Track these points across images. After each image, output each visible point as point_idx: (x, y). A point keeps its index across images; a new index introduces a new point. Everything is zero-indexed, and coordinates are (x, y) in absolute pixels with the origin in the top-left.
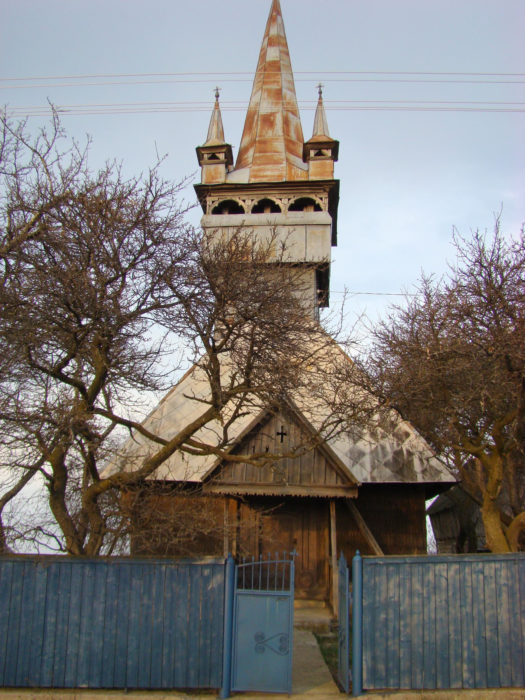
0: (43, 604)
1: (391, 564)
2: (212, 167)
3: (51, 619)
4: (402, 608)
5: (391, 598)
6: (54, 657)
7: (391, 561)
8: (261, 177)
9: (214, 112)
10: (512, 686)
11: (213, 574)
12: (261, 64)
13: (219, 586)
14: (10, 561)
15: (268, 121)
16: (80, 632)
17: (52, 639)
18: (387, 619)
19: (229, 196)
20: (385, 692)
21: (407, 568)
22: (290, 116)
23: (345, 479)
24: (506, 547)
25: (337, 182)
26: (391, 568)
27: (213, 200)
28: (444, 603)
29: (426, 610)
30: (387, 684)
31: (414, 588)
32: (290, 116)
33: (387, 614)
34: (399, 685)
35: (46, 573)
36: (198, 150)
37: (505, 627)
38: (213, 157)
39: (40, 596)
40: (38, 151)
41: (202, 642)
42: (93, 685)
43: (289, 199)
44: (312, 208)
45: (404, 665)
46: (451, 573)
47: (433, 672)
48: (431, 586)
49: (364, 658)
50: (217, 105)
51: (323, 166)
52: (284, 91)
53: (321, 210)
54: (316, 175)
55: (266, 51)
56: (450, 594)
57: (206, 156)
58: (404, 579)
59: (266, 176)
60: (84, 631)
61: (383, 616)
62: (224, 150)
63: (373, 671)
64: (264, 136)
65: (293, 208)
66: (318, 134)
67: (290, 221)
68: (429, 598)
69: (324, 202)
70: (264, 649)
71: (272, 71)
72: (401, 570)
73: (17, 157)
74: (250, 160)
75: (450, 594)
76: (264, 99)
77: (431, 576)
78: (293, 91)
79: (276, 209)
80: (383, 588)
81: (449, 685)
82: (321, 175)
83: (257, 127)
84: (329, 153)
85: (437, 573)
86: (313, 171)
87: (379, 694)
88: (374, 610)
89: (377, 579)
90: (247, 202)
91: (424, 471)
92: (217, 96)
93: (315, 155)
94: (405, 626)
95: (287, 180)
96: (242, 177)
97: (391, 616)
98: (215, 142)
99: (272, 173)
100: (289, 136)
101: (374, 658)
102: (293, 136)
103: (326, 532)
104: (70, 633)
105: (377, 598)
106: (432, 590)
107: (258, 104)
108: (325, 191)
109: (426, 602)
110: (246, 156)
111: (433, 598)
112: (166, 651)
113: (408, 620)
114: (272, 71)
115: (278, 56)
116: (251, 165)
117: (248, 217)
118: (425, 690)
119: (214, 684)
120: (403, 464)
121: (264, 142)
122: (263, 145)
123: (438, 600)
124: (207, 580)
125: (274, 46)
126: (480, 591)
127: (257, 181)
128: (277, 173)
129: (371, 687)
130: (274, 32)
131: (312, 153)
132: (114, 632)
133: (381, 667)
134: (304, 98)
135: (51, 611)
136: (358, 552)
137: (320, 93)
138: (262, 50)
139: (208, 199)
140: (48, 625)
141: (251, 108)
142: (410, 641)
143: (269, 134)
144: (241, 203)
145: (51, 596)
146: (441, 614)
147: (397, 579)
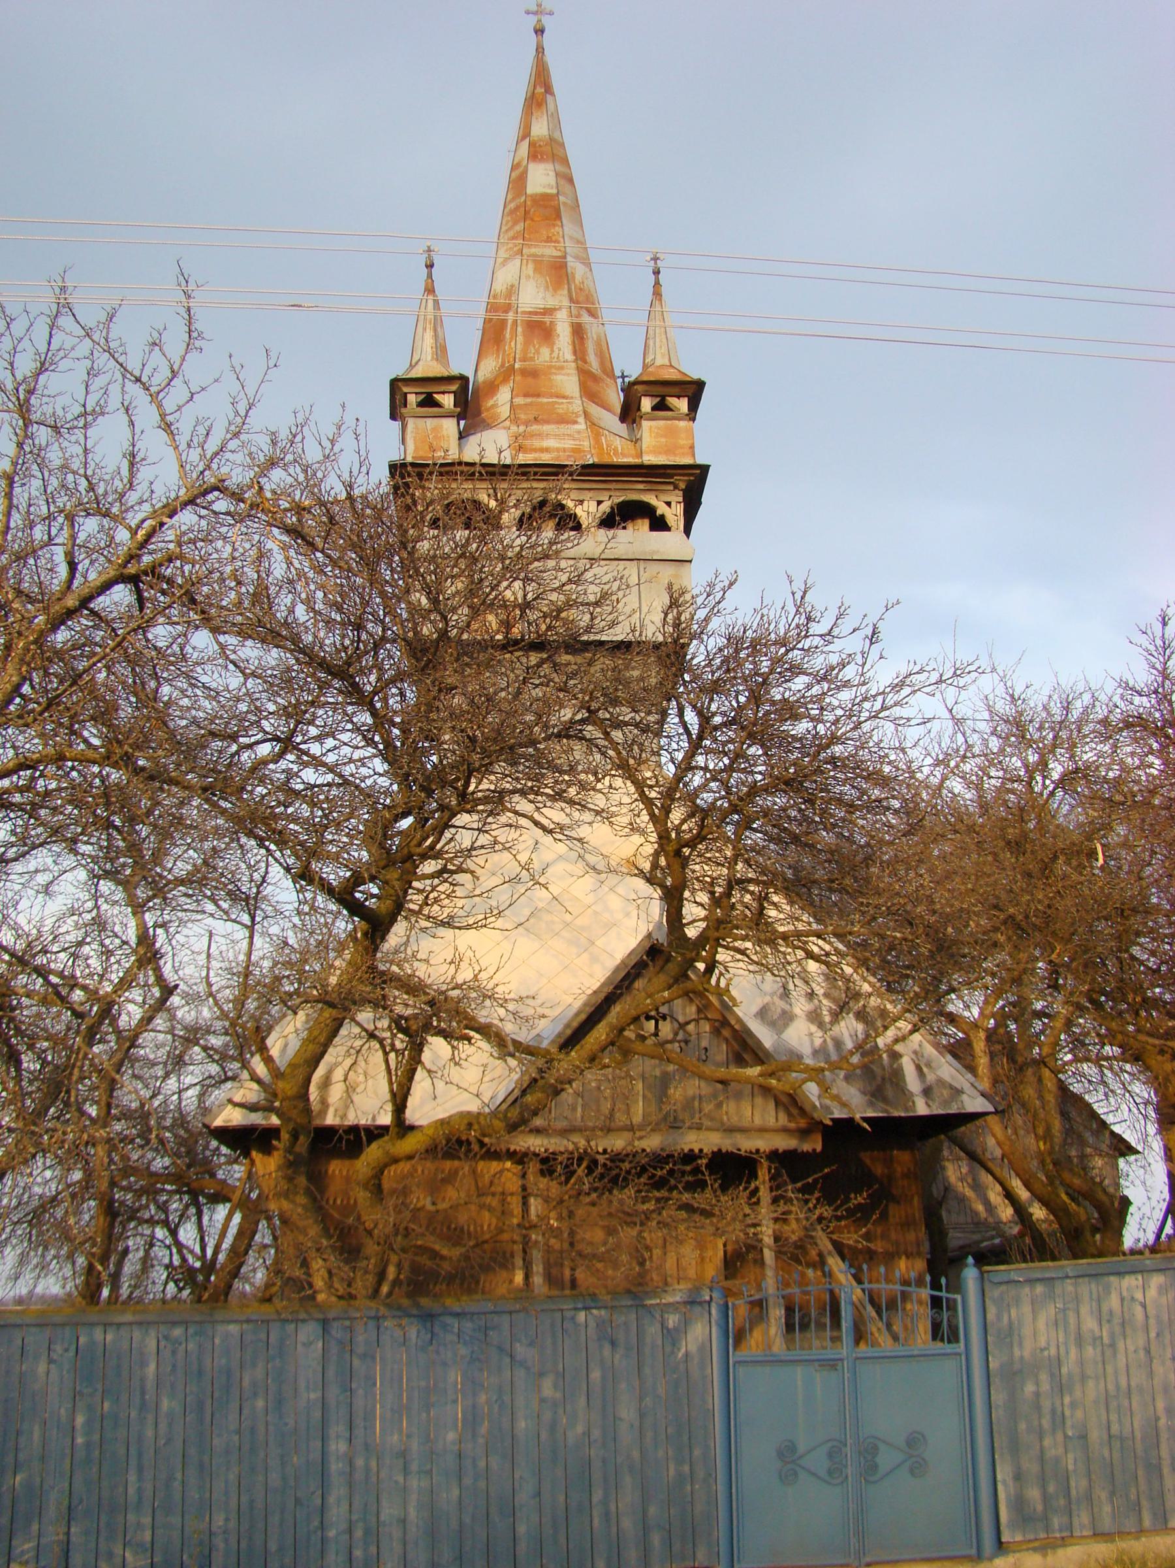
0: (317, 1414)
1: (1038, 1280)
2: (430, 423)
3: (337, 1446)
4: (1064, 1370)
5: (1042, 1350)
6: (350, 1531)
7: (1039, 1275)
8: (535, 450)
11: (686, 1322)
12: (513, 199)
13: (701, 1348)
14: (235, 1321)
15: (540, 328)
16: (406, 1471)
17: (343, 1491)
18: (1037, 1394)
20: (1045, 1547)
21: (1069, 1286)
22: (586, 318)
23: (795, 1111)
25: (704, 470)
28: (1142, 1354)
29: (1110, 1369)
30: (1047, 1529)
31: (1084, 1328)
32: (586, 318)
33: (1037, 1384)
34: (1071, 1527)
35: (320, 1344)
36: (395, 384)
38: (429, 402)
40: (145, 379)
41: (672, 1472)
43: (599, 503)
44: (646, 522)
45: (1078, 1485)
46: (1152, 1292)
47: (1133, 1497)
48: (1117, 1320)
49: (999, 1477)
51: (671, 433)
53: (667, 528)
54: (656, 451)
55: (526, 171)
56: (1153, 1335)
57: (412, 399)
58: (1064, 1310)
59: (547, 450)
60: (414, 1467)
62: (454, 388)
63: (1019, 1504)
64: (532, 359)
65: (608, 522)
66: (659, 362)
68: (1113, 1345)
69: (674, 513)
70: (796, 1474)
71: (537, 216)
72: (1058, 1290)
73: (91, 389)
74: (504, 411)
75: (1153, 1335)
76: (528, 277)
77: (1114, 1302)
78: (587, 263)
80: (1027, 1331)
81: (1166, 1521)
82: (668, 451)
83: (516, 343)
84: (683, 405)
85: (1125, 1294)
86: (654, 442)
87: (1035, 1549)
88: (1014, 1374)
89: (1013, 1312)
91: (927, 1092)
92: (430, 266)
93: (654, 408)
94: (1073, 1405)
95: (596, 460)
96: (491, 445)
97: (1045, 1386)
99: (557, 444)
100: (585, 362)
101: (1018, 1477)
102: (594, 364)
104: (383, 1474)
105: (1017, 1353)
106: (1117, 1329)
107: (512, 290)
108: (676, 487)
109: (1108, 1352)
110: (491, 403)
111: (1121, 1345)
112: (598, 1496)
113: (1078, 1393)
114: (537, 216)
115: (553, 183)
116: (507, 423)
117: (594, 541)
120: (883, 1079)
121: (532, 373)
122: (530, 380)
123: (1131, 1348)
124: (672, 1337)
125: (542, 160)
127: (523, 458)
128: (569, 444)
129: (1019, 1538)
130: (540, 129)
131: (646, 404)
132: (482, 1464)
133: (1034, 1493)
135: (338, 1429)
136: (970, 1260)
137: (657, 272)
138: (514, 168)
140: (332, 1459)
141: (495, 297)
142: (1084, 1437)
143: (544, 355)
145: (333, 1392)
146: (1138, 1377)
147: (1052, 1311)
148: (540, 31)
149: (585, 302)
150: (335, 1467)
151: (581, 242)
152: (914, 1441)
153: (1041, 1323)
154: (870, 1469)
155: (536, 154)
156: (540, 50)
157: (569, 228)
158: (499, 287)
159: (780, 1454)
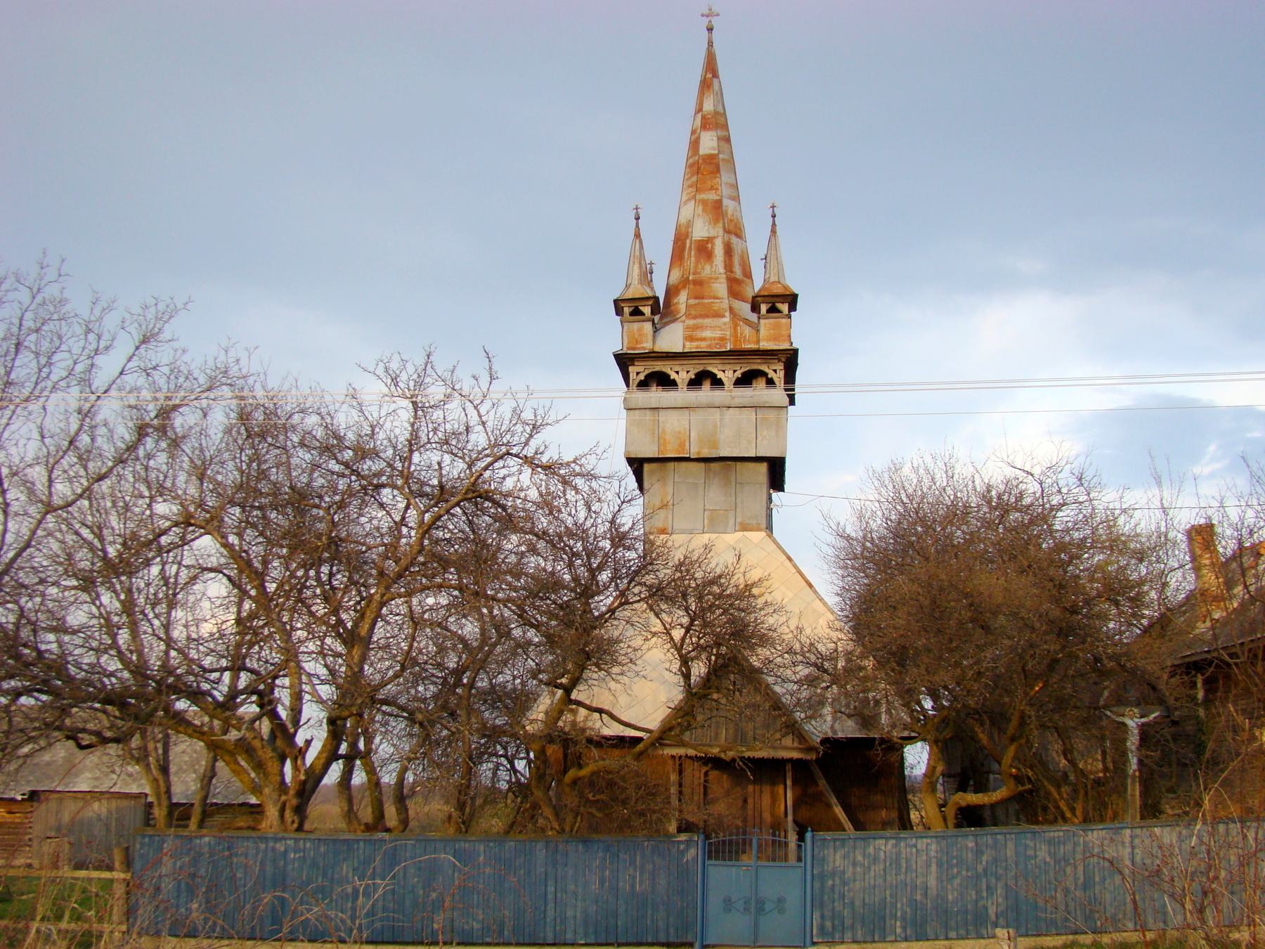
2: (636, 326)
3: (551, 889)
8: (698, 340)
9: (634, 243)
10: (937, 939)
11: (687, 849)
15: (704, 249)
19: (659, 366)
22: (734, 239)
24: (942, 824)
25: (796, 351)
26: (838, 843)
27: (638, 371)
30: (833, 937)
36: (616, 302)
37: (933, 891)
38: (636, 312)
39: (540, 870)
42: (589, 941)
45: (847, 922)
46: (889, 846)
50: (637, 235)
52: (726, 202)
54: (768, 340)
55: (699, 138)
59: (703, 339)
61: (830, 882)
63: (822, 928)
66: (772, 279)
67: (737, 402)
68: (869, 868)
69: (779, 377)
74: (682, 308)
77: (871, 850)
78: (736, 198)
79: (717, 383)
80: (831, 859)
83: (691, 260)
86: (766, 335)
90: (682, 374)
97: (837, 882)
98: (637, 291)
101: (822, 917)
103: (781, 791)
107: (690, 224)
112: (649, 912)
114: (706, 170)
118: (865, 942)
119: (690, 939)
121: (699, 283)
124: (683, 853)
125: (709, 129)
126: (913, 862)
128: (718, 334)
130: (708, 106)
131: (764, 308)
133: (828, 924)
134: (755, 245)
135: (551, 883)
137: (774, 216)
139: (631, 369)
142: (852, 903)
143: (707, 271)
144: (673, 376)
146: (880, 881)
148: (710, 29)
149: (735, 230)
150: (550, 897)
151: (735, 187)
152: (781, 900)
153: (838, 857)
154: (760, 909)
155: (706, 124)
156: (710, 44)
157: (725, 177)
158: (683, 220)
159: (724, 901)
